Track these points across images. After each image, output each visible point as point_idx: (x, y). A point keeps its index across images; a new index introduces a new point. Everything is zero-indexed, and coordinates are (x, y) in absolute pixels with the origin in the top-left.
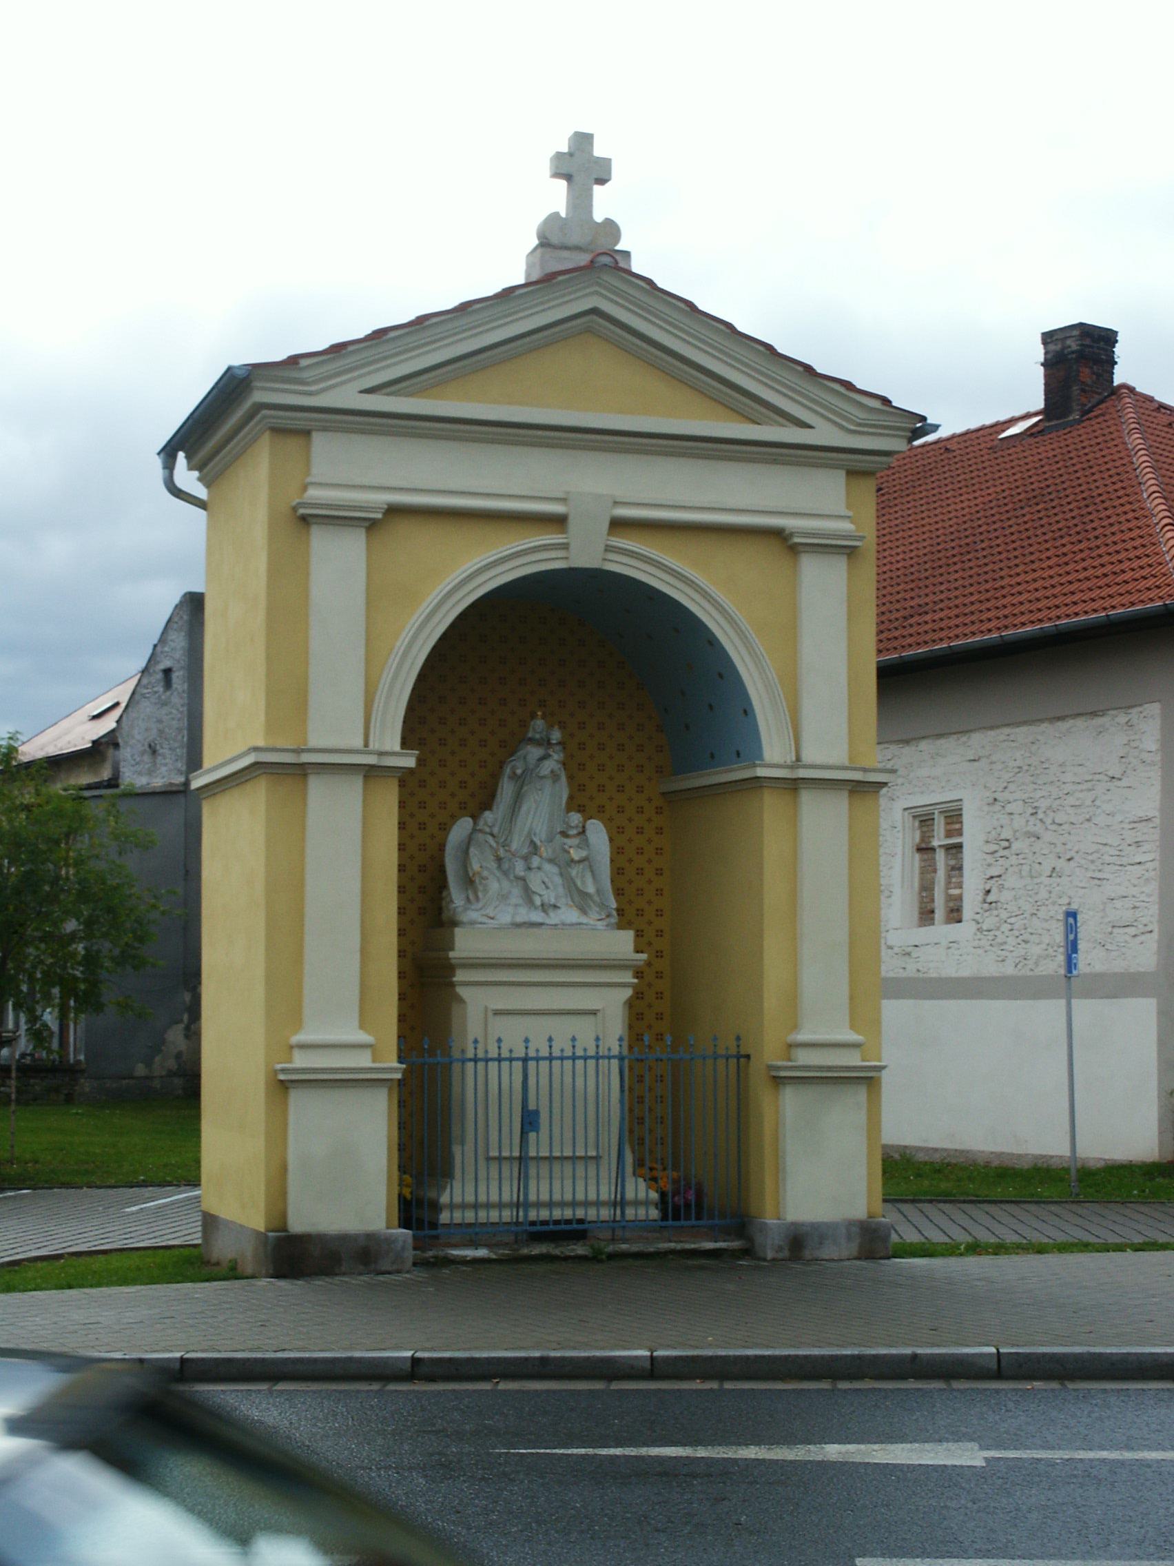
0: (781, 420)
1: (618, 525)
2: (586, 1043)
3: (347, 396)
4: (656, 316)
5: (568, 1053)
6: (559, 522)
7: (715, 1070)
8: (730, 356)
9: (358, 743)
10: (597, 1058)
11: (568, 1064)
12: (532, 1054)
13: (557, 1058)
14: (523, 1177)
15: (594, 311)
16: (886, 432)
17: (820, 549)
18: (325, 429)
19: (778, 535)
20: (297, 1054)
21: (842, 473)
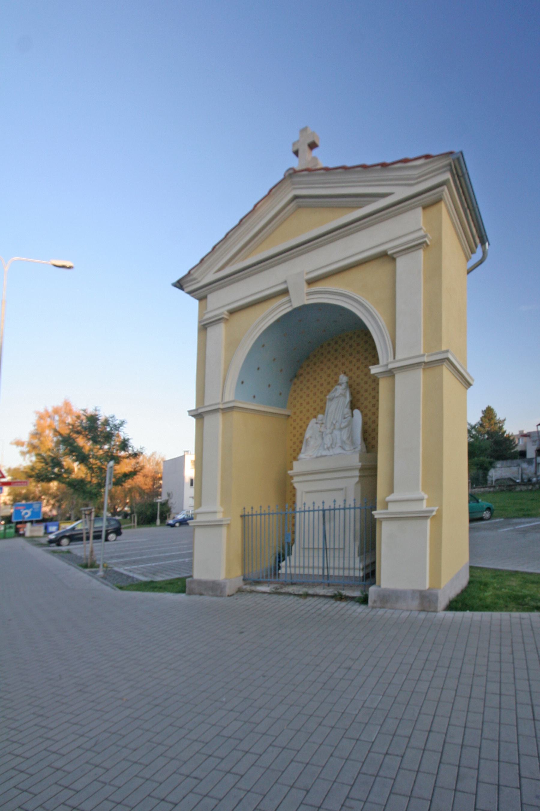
0: (371, 199)
1: (311, 282)
2: (340, 503)
3: (211, 277)
4: (316, 183)
5: (311, 509)
6: (285, 292)
7: (256, 520)
8: (349, 182)
9: (220, 400)
10: (344, 509)
11: (311, 513)
12: (347, 506)
13: (348, 508)
14: (325, 557)
15: (296, 197)
16: (431, 175)
17: (407, 252)
18: (210, 293)
19: (384, 255)
20: (390, 506)
21: (420, 210)
